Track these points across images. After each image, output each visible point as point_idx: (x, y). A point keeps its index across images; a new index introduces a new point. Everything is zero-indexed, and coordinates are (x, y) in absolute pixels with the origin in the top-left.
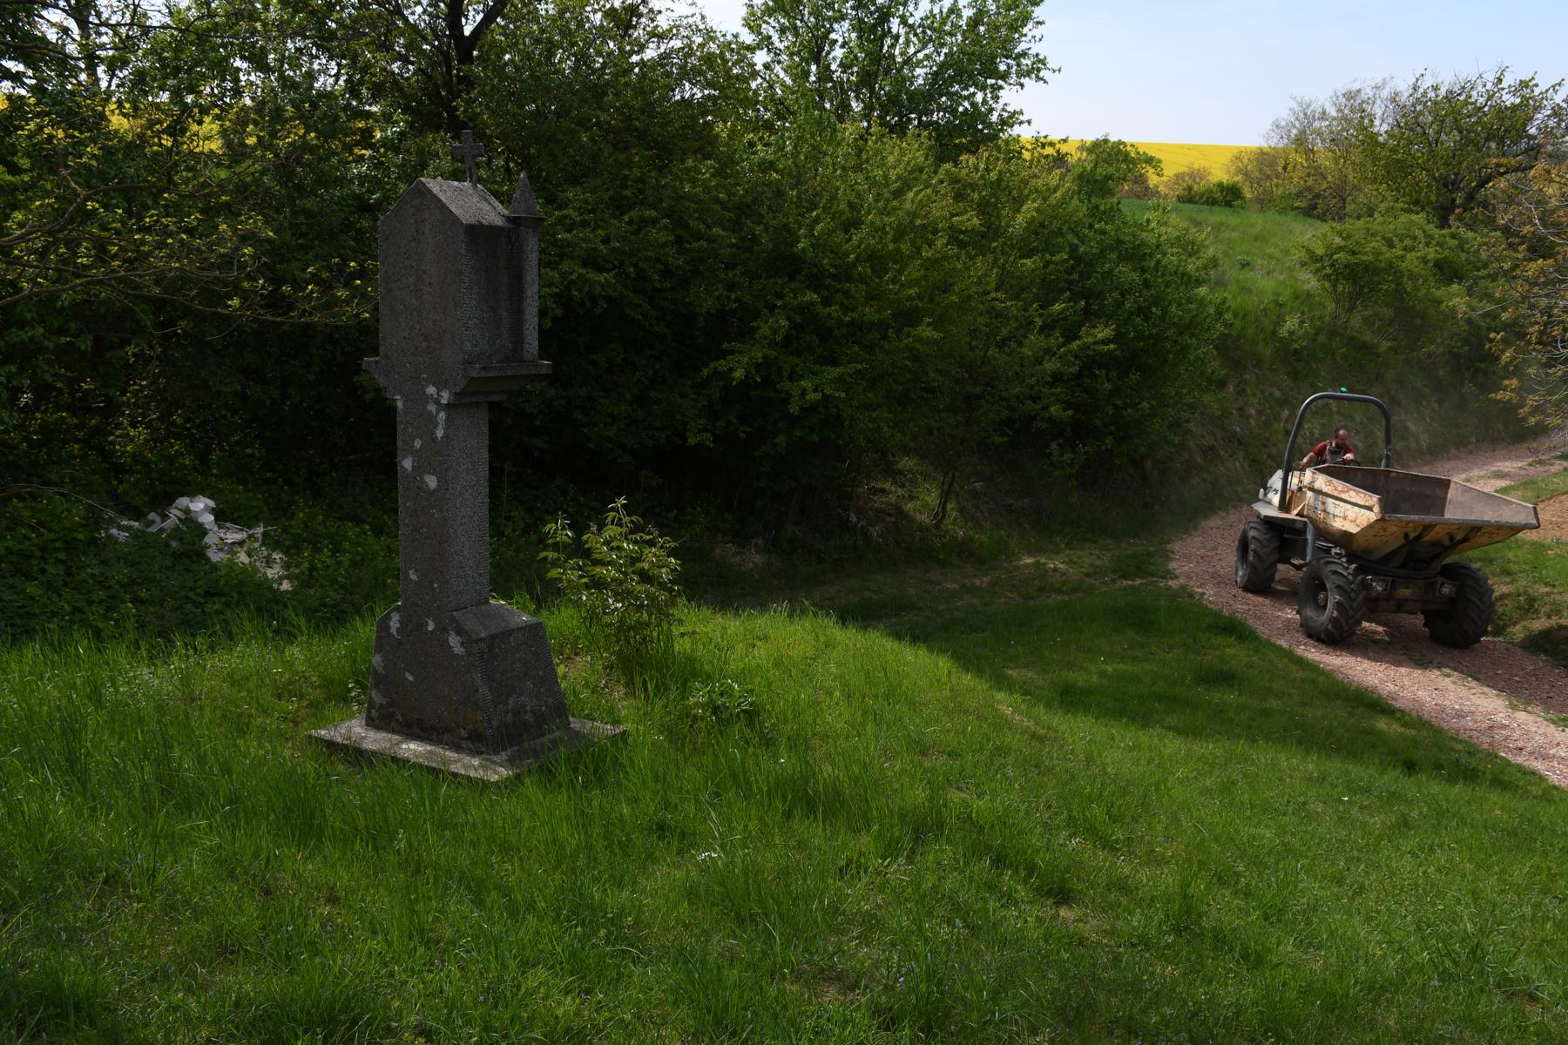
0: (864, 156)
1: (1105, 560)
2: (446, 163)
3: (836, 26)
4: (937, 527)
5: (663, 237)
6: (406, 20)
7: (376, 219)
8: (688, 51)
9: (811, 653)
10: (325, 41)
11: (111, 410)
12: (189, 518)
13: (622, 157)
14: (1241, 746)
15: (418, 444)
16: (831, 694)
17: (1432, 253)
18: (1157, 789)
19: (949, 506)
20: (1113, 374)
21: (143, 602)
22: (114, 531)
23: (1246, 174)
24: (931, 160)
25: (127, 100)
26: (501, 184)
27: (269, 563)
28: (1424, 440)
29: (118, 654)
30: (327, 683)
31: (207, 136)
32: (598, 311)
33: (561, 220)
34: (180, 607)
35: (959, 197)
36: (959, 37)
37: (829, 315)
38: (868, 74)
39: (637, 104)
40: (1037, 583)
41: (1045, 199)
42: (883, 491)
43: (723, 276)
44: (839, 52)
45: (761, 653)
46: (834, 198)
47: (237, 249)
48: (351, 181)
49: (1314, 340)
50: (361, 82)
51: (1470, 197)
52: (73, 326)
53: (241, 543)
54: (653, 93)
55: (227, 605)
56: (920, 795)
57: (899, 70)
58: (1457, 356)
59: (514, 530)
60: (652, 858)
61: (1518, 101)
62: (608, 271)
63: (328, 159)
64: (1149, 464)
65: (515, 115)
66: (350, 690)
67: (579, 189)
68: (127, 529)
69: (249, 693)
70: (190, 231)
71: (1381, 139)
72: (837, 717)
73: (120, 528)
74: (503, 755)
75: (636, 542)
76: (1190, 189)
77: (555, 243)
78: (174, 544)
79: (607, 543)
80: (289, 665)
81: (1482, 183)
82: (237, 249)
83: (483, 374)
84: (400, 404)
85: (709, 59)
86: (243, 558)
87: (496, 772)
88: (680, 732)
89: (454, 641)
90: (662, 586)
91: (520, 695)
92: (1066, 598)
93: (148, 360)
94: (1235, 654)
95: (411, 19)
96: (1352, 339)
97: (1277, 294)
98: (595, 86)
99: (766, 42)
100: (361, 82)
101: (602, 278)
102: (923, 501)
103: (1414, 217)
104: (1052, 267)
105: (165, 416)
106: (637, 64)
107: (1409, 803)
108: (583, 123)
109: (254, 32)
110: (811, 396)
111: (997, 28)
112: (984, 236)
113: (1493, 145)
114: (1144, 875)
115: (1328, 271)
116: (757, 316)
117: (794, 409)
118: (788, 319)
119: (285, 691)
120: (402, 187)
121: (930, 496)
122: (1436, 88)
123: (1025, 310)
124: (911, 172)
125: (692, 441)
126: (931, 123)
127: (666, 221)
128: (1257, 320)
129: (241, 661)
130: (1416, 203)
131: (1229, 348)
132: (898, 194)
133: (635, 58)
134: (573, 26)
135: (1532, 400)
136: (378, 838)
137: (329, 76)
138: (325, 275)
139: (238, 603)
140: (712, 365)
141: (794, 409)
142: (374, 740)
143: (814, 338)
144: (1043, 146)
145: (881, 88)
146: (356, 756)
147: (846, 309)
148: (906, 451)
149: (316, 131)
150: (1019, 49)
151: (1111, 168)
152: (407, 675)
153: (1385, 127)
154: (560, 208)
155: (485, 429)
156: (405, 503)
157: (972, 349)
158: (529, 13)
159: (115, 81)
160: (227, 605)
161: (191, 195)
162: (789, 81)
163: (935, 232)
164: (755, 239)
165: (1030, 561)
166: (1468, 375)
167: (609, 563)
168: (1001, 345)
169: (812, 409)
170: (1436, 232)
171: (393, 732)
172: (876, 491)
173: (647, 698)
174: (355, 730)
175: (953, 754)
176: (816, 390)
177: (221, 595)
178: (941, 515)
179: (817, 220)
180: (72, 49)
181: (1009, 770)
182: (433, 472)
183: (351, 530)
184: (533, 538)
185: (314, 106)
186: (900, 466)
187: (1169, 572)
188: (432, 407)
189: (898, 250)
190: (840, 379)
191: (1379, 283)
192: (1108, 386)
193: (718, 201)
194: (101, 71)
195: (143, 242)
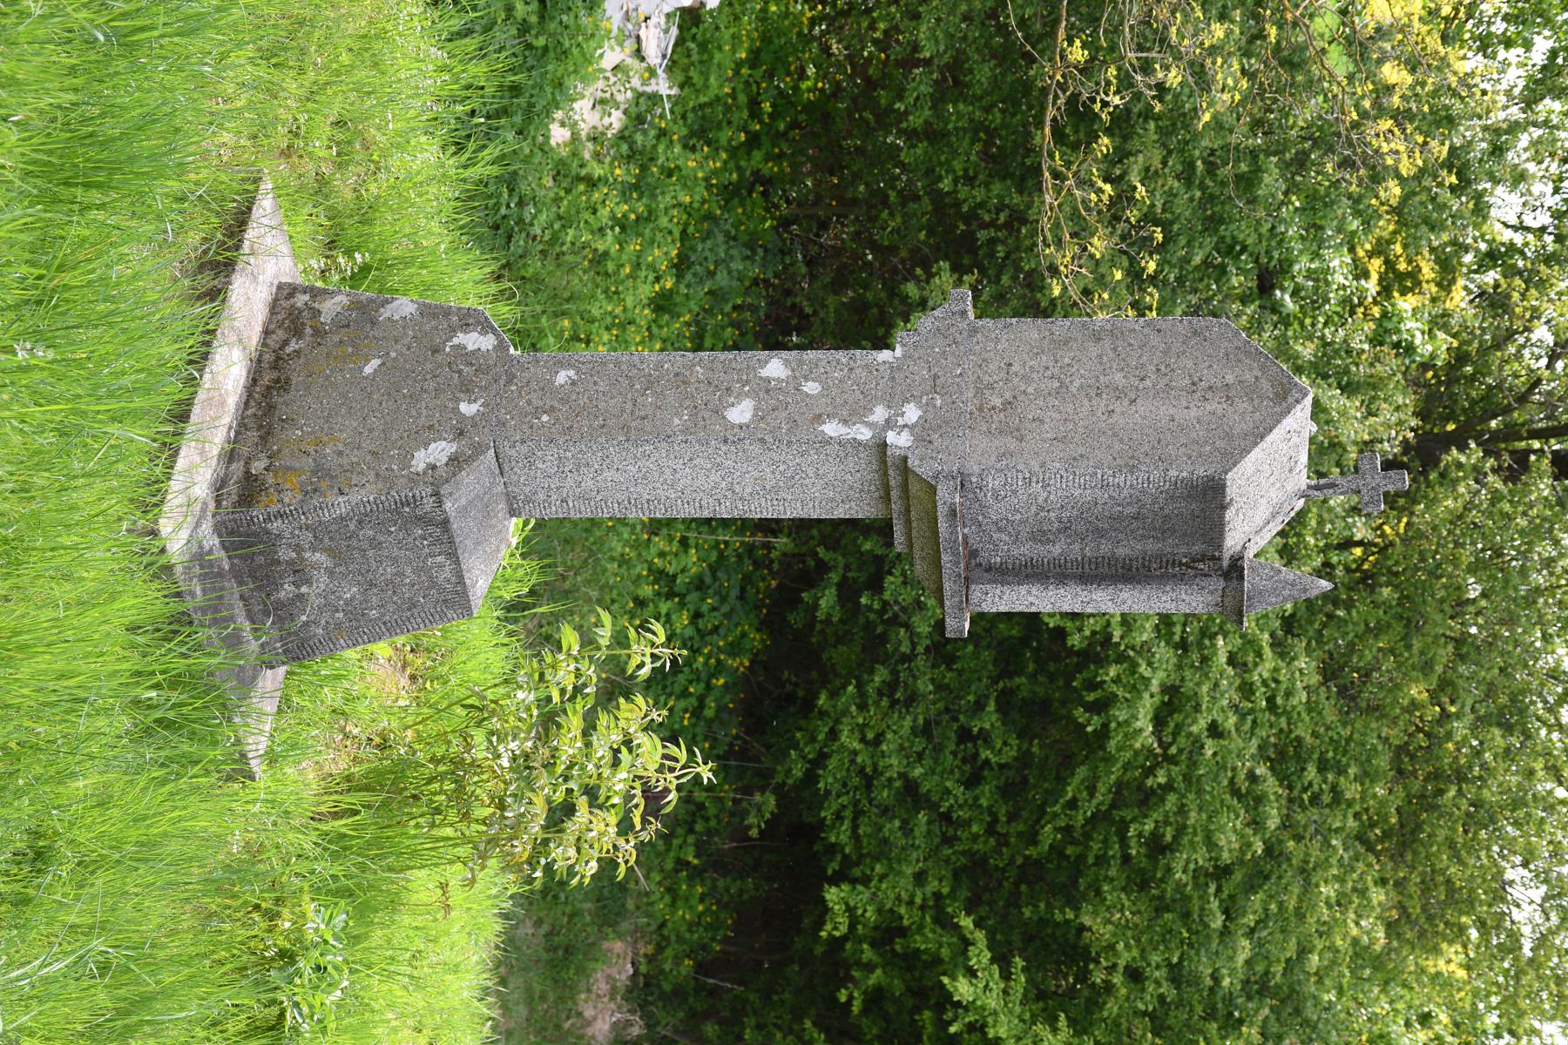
2: (1353, 430)
5: (1228, 842)
13: (1383, 762)
15: (812, 388)
27: (601, 103)
30: (366, 213)
32: (1080, 714)
33: (1250, 643)
39: (1490, 795)
43: (1155, 958)
47: (1178, 57)
48: (1316, 255)
50: (1511, 272)
53: (639, 54)
55: (524, 28)
59: (662, 554)
62: (1157, 732)
63: (1357, 213)
65: (1455, 561)
66: (349, 253)
67: (1315, 679)
74: (212, 541)
75: (629, 797)
77: (1205, 633)
79: (628, 743)
80: (401, 143)
82: (1178, 57)
83: (942, 511)
84: (885, 355)
87: (178, 528)
88: (246, 885)
89: (439, 451)
98: (1522, 712)
101: (1144, 723)
108: (1445, 688)
119: (349, 136)
120: (1307, 351)
125: (832, 894)
127: (1259, 848)
138: (1133, 215)
140: (980, 936)
142: (248, 303)
146: (216, 268)
149: (1405, 199)
152: (375, 363)
154: (1276, 644)
155: (839, 513)
156: (700, 365)
160: (524, 28)
171: (267, 332)
173: (317, 818)
174: (273, 260)
177: (542, 18)
182: (759, 417)
183: (663, 254)
184: (647, 591)
188: (879, 414)
193: (1303, 952)
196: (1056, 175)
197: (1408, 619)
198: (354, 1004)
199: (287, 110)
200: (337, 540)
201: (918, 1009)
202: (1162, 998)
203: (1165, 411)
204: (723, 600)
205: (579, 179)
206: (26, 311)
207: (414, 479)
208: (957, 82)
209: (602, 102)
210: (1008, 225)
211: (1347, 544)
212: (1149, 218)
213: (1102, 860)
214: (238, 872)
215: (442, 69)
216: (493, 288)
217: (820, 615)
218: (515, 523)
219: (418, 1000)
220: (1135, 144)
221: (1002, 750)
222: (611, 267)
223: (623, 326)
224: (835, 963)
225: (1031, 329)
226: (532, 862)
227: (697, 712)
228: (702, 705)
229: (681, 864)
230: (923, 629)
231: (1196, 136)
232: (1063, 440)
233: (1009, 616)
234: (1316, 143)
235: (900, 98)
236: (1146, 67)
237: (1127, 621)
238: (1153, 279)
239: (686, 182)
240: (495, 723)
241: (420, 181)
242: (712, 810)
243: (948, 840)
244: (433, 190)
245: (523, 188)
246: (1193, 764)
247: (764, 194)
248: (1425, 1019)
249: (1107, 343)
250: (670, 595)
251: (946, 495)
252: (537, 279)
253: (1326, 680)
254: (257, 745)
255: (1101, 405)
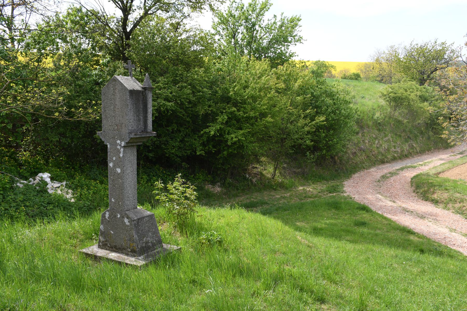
0: (249, 67)
1: (324, 187)
2: (122, 70)
3: (239, 28)
4: (273, 178)
5: (189, 91)
6: (109, 27)
7: (100, 87)
8: (195, 36)
9: (238, 221)
10: (85, 33)
11: (18, 147)
12: (42, 180)
13: (176, 67)
14: (370, 246)
15: (114, 159)
16: (245, 234)
17: (419, 93)
18: (347, 262)
19: (276, 172)
20: (325, 131)
21: (27, 206)
22: (18, 184)
23: (361, 70)
24: (269, 67)
25: (24, 52)
26: (139, 76)
27: (67, 193)
28: (418, 149)
29: (18, 226)
30: (85, 233)
31: (48, 63)
33: (157, 87)
34: (39, 208)
35: (278, 78)
36: (277, 31)
37: (240, 115)
38: (249, 42)
40: (304, 195)
41: (304, 79)
42: (256, 168)
43: (207, 103)
44: (240, 36)
45: (223, 220)
46: (241, 79)
47: (57, 98)
48: (93, 76)
49: (384, 120)
50: (96, 46)
51: (429, 76)
52: (6, 121)
53: (59, 187)
54: (185, 48)
55: (54, 207)
56: (275, 268)
57: (258, 41)
58: (427, 124)
59: (144, 182)
60: (191, 292)
61: (441, 48)
62: (172, 102)
63: (86, 69)
64: (336, 158)
65: (143, 55)
67: (163, 77)
68: (23, 183)
69: (59, 239)
70: (43, 92)
71: (401, 60)
72: (247, 242)
73: (21, 183)
75: (184, 187)
76: (345, 75)
77: (156, 94)
78: (37, 188)
79: (175, 187)
81: (432, 73)
83: (135, 137)
84: (108, 146)
85: (201, 38)
86: (59, 192)
88: (199, 249)
89: (126, 221)
90: (192, 201)
91: (147, 237)
92: (313, 199)
93: (29, 131)
94: (365, 216)
95: (111, 27)
96: (396, 119)
97: (373, 106)
98: (167, 46)
99: (219, 33)
100: (96, 46)
101: (170, 104)
102: (268, 170)
103: (412, 83)
104: (306, 99)
105: (35, 148)
106: (180, 40)
107: (424, 263)
108: (164, 58)
109: (63, 31)
110: (235, 139)
111: (288, 28)
112: (285, 90)
113: (434, 61)
114: (347, 293)
115: (388, 99)
116: (218, 115)
117: (229, 143)
118: (227, 116)
120: (109, 77)
121: (271, 169)
122: (417, 45)
123: (299, 112)
124: (263, 71)
125: (198, 153)
126: (268, 57)
127: (189, 87)
128: (367, 114)
129: (59, 226)
130: (413, 78)
131: (359, 122)
132: (259, 78)
133: (179, 38)
134: (160, 28)
135: (452, 137)
136: (102, 288)
137: (86, 44)
139: (57, 206)
140: (204, 130)
141: (229, 143)
142: (101, 253)
143: (235, 122)
144: (302, 63)
145: (253, 46)
146: (96, 258)
147: (245, 113)
148: (263, 155)
149: (83, 61)
150: (294, 34)
151: (321, 70)
152: (111, 232)
153: (402, 57)
154: (157, 83)
155: (136, 154)
156: (110, 178)
157: (282, 124)
158: (147, 24)
159: (20, 46)
160: (54, 207)
161: (43, 81)
162: (225, 44)
163: (271, 89)
164: (216, 92)
165: (301, 188)
166: (430, 129)
167: (175, 194)
168: (291, 123)
169: (235, 143)
170: (419, 87)
171: (106, 249)
172: (254, 168)
174: (94, 249)
175: (284, 253)
176: (236, 138)
177: (53, 204)
178: (274, 175)
179: (235, 86)
180: (7, 37)
181: (302, 258)
182: (119, 167)
183: (93, 183)
184: (150, 184)
185: (82, 53)
186: (261, 160)
187: (344, 191)
188: (119, 147)
189: (260, 95)
190: (243, 134)
191: (403, 102)
192: (324, 135)
193: (205, 81)
194: (16, 43)
195: (28, 96)
196: (78, 118)
197: (153, 63)
198: (217, 229)
199: (68, 247)
200: (141, 236)
201: (215, 140)
202: (213, 102)
203: (118, 99)
204: (151, 172)
205: (80, 197)
206: (103, 291)
207: (131, 224)
208: (63, 134)
209: (67, 193)
210: (87, 126)
211: (141, 72)
212: (86, 102)
213: (192, 111)
214: (196, 249)
215: (61, 222)
216: (98, 212)
217: (153, 156)
218: (138, 207)
219: (216, 219)
220: (74, 105)
221: (175, 127)
222: (95, 191)
223: (105, 189)
224: (209, 153)
225: (104, 122)
226: (194, 202)
227: (169, 175)
228: (168, 175)
229: (193, 177)
230: (155, 139)
231: (72, 95)
232: (123, 117)
233: (153, 126)
234: (74, 75)
235: (66, 143)
236: (59, 103)
237: (154, 106)
238: (96, 102)
239: (80, 179)
240: (172, 209)
241: (79, 225)
242: (185, 173)
243: (189, 135)
244: (81, 222)
245: (82, 206)
246: (176, 96)
247: (83, 166)
248: (214, 63)
249: (106, 109)
250: (150, 180)
251: (132, 136)
252: (97, 204)
253: (163, 76)
254: (175, 247)
255: (117, 110)
